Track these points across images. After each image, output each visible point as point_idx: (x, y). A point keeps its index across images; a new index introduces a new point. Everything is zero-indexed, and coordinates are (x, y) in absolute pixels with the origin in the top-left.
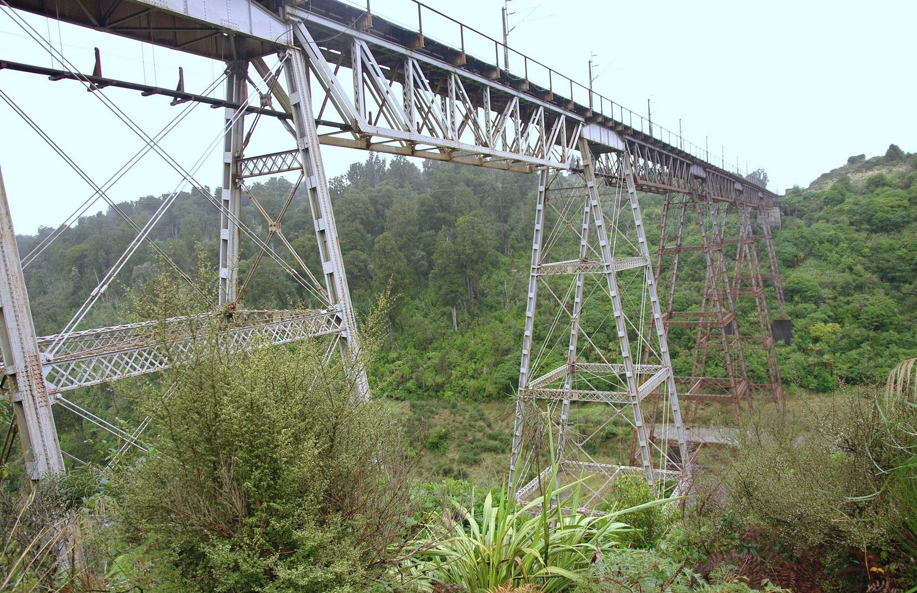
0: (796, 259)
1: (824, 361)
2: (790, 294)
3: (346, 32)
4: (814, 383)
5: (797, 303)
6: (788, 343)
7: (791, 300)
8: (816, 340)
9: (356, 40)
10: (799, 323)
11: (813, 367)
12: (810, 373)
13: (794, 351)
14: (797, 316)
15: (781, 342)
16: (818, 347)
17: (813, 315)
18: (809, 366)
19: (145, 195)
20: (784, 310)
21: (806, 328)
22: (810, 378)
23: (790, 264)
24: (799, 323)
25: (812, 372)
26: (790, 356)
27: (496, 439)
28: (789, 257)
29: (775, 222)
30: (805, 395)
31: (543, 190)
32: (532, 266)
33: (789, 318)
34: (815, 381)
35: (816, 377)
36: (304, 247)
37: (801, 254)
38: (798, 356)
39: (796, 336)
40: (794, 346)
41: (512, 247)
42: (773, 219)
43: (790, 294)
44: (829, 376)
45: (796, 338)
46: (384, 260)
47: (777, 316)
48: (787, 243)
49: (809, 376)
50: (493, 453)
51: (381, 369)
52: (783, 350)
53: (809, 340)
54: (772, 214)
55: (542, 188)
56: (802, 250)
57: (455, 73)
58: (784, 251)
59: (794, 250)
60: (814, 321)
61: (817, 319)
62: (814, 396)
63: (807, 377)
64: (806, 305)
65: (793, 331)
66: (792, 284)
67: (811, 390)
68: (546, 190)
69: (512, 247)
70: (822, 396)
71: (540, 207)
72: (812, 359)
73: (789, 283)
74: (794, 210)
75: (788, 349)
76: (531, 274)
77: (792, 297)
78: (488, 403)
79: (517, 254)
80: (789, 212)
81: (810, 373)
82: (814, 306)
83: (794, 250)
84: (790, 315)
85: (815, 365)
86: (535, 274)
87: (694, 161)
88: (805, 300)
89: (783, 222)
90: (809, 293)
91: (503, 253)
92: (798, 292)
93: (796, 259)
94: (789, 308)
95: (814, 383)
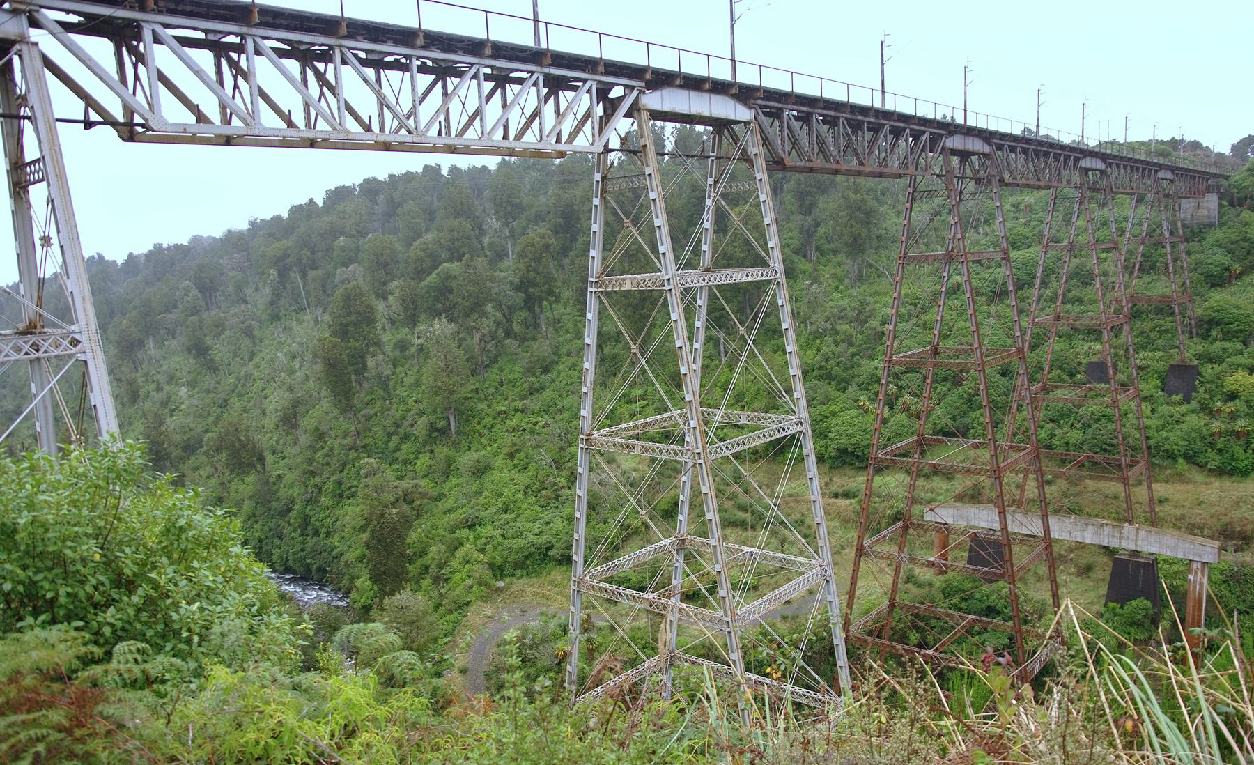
0: (1227, 274)
1: (1236, 428)
2: (1206, 326)
3: (114, 15)
4: (1214, 460)
5: (1216, 339)
6: (1187, 400)
7: (1205, 336)
8: (1232, 396)
9: (143, 24)
10: (1209, 370)
11: (1217, 437)
12: (1212, 445)
13: (1193, 411)
14: (1211, 361)
15: (1176, 398)
16: (1229, 407)
17: (1233, 359)
18: (1213, 435)
19: (340, 183)
20: (1191, 349)
21: (1219, 378)
22: (1211, 454)
23: (1217, 281)
24: (1209, 370)
25: (1215, 445)
26: (1184, 419)
27: (746, 511)
28: (1216, 271)
29: (1209, 216)
30: (1198, 476)
31: (599, 179)
32: (590, 279)
33: (1196, 362)
34: (1218, 458)
35: (1220, 451)
36: (533, 245)
37: (1237, 267)
38: (1196, 421)
39: (1202, 390)
40: (1194, 404)
41: (818, 249)
42: (1205, 212)
43: (1206, 326)
44: (1241, 451)
45: (1201, 393)
46: (627, 265)
47: (1176, 360)
48: (1216, 250)
49: (1210, 450)
50: (739, 528)
51: (620, 411)
52: (1177, 410)
53: (1219, 397)
54: (1205, 204)
55: (598, 177)
56: (1239, 260)
57: (341, 46)
58: (1210, 261)
59: (1226, 259)
60: (1233, 368)
61: (1239, 365)
62: (1213, 479)
63: (1206, 451)
64: (1226, 344)
65: (1197, 382)
66: (1209, 312)
67: (1210, 470)
68: (603, 178)
69: (818, 249)
70: (1227, 483)
71: (596, 201)
72: (1216, 425)
73: (1206, 309)
74: (1246, 199)
75: (1184, 408)
76: (589, 289)
77: (1208, 330)
78: (754, 462)
79: (823, 260)
80: (1236, 201)
81: (1212, 445)
82: (1239, 346)
83: (1226, 259)
84: (1199, 357)
85: (1220, 434)
86: (593, 290)
87: (949, 128)
88: (1227, 336)
89: (1221, 216)
90: (1234, 327)
91: (805, 257)
92: (1218, 323)
93: (1227, 274)
94: (1197, 346)
95: (1214, 460)
